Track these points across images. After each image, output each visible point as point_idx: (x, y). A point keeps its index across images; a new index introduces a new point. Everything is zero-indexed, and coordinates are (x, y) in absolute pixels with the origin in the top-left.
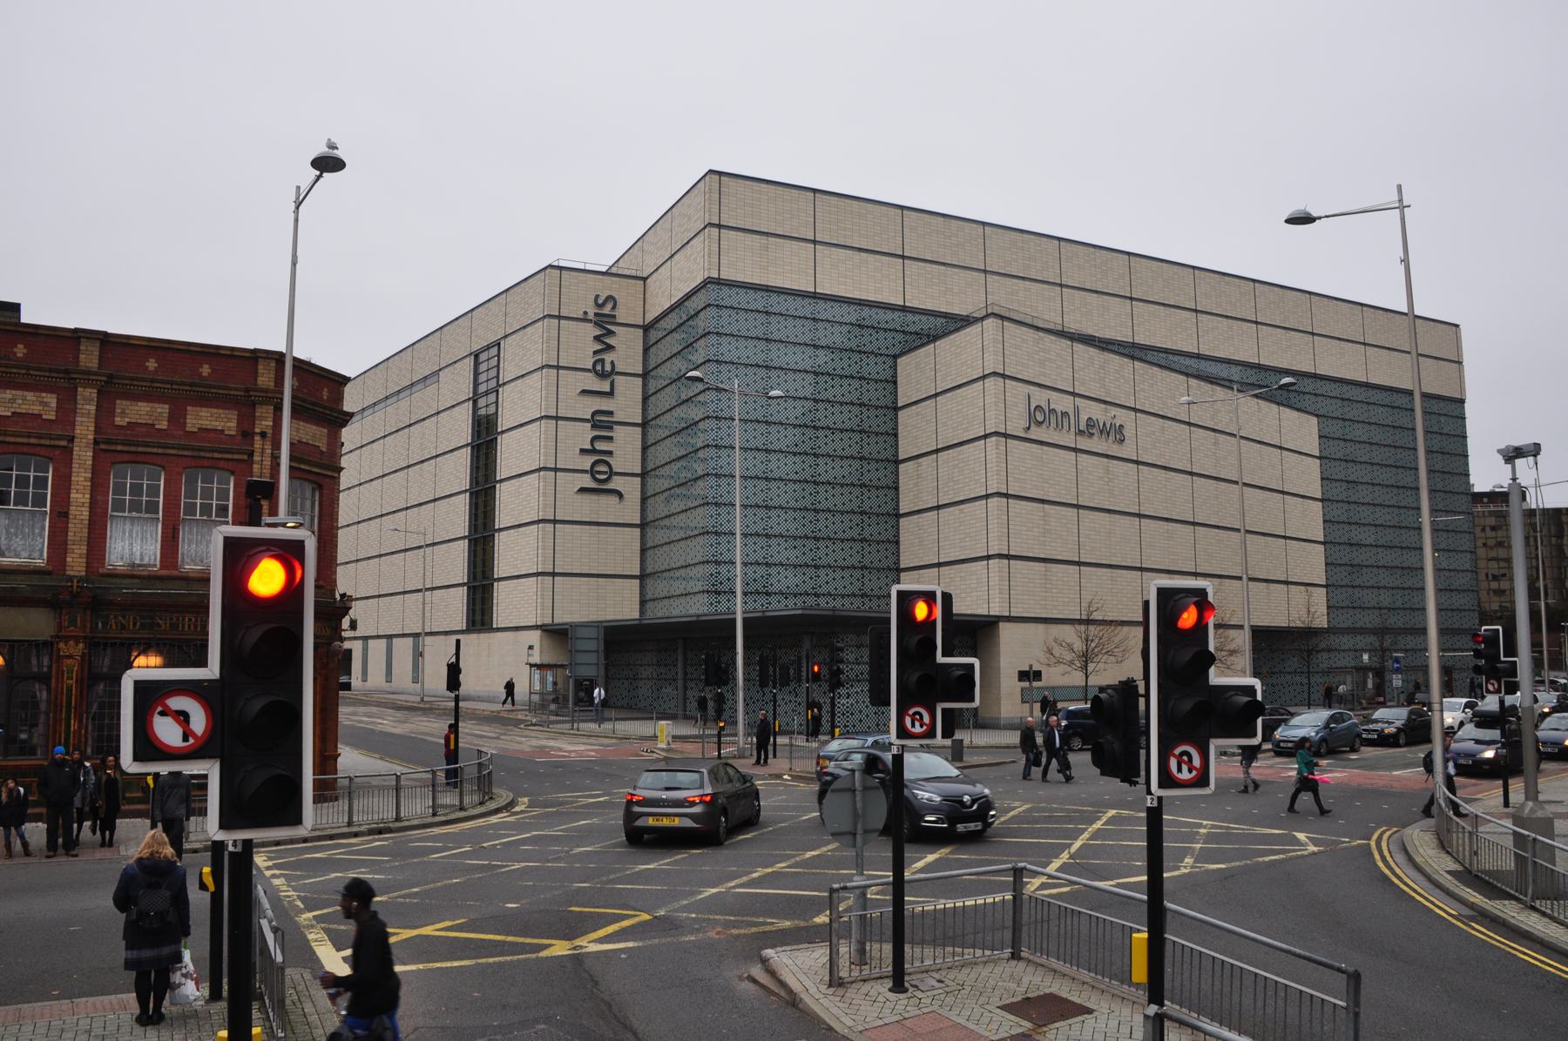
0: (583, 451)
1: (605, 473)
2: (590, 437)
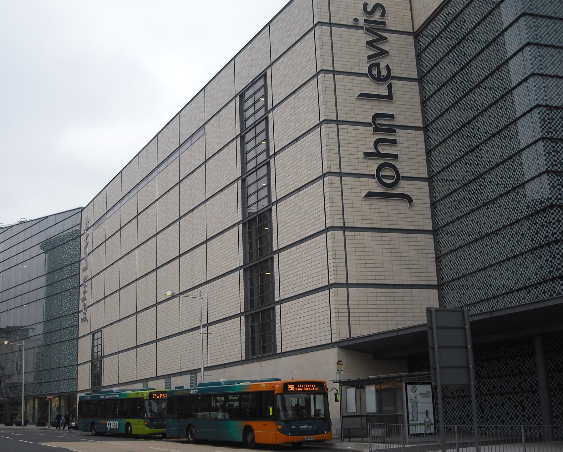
0: (367, 155)
1: (392, 177)
2: (373, 140)
